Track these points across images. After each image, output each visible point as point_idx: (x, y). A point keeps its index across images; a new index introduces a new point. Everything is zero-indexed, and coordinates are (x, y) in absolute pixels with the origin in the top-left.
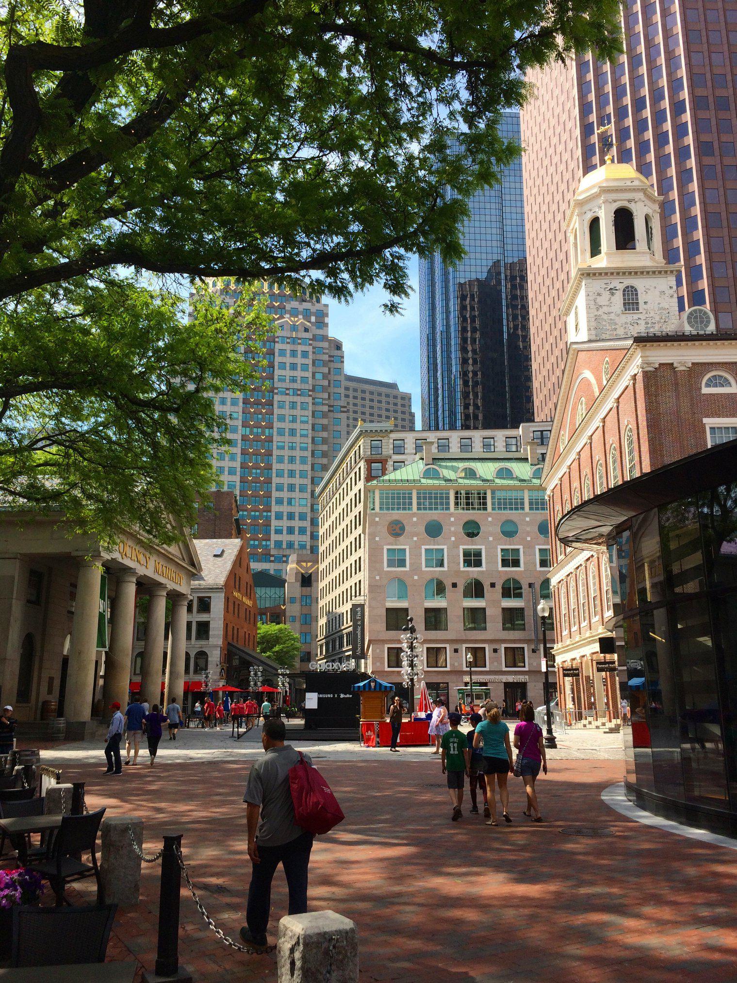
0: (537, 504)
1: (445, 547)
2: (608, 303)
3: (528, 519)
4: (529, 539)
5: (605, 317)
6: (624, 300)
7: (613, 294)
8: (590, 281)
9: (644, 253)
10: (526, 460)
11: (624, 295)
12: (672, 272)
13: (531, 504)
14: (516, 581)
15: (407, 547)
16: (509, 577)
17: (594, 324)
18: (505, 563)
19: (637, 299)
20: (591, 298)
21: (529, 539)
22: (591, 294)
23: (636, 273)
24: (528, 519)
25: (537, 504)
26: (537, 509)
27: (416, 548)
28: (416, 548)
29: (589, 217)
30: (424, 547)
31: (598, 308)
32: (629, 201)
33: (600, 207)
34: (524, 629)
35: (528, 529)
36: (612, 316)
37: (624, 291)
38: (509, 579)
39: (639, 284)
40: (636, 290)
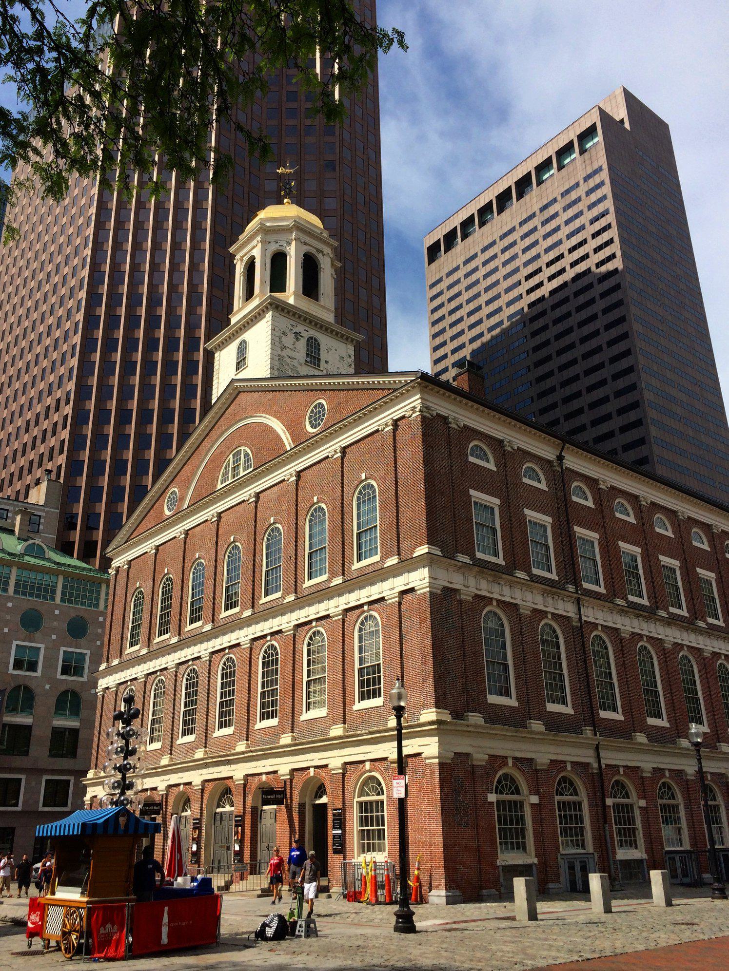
0: (25, 586)
1: (42, 646)
2: (292, 347)
3: (10, 605)
4: (6, 630)
5: (288, 360)
6: (308, 350)
7: (297, 339)
8: (277, 314)
9: (328, 309)
10: (12, 532)
11: (308, 345)
12: (352, 340)
13: (17, 585)
14: (27, 689)
15: (42, 646)
16: (69, 687)
17: (277, 363)
18: (18, 665)
19: (319, 355)
20: (278, 334)
21: (6, 630)
22: (277, 329)
23: (321, 327)
24: (10, 605)
25: (25, 586)
26: (24, 594)
27: (55, 647)
28: (52, 649)
29: (273, 248)
30: (15, 643)
31: (284, 347)
32: (318, 250)
33: (289, 244)
34: (667, 905)
35: (8, 617)
36: (295, 363)
37: (308, 340)
38: (19, 687)
39: (325, 341)
40: (319, 344)
